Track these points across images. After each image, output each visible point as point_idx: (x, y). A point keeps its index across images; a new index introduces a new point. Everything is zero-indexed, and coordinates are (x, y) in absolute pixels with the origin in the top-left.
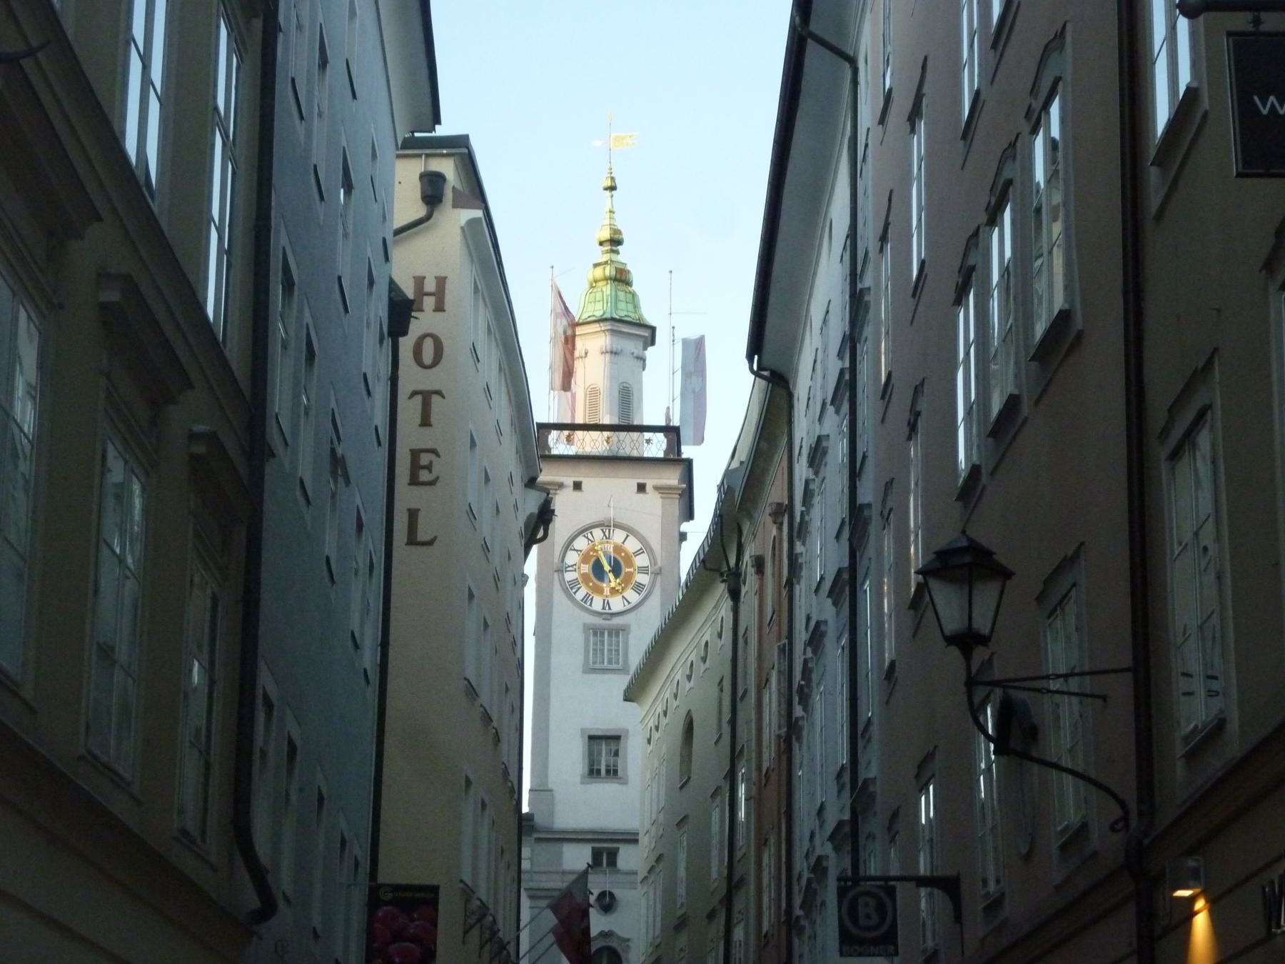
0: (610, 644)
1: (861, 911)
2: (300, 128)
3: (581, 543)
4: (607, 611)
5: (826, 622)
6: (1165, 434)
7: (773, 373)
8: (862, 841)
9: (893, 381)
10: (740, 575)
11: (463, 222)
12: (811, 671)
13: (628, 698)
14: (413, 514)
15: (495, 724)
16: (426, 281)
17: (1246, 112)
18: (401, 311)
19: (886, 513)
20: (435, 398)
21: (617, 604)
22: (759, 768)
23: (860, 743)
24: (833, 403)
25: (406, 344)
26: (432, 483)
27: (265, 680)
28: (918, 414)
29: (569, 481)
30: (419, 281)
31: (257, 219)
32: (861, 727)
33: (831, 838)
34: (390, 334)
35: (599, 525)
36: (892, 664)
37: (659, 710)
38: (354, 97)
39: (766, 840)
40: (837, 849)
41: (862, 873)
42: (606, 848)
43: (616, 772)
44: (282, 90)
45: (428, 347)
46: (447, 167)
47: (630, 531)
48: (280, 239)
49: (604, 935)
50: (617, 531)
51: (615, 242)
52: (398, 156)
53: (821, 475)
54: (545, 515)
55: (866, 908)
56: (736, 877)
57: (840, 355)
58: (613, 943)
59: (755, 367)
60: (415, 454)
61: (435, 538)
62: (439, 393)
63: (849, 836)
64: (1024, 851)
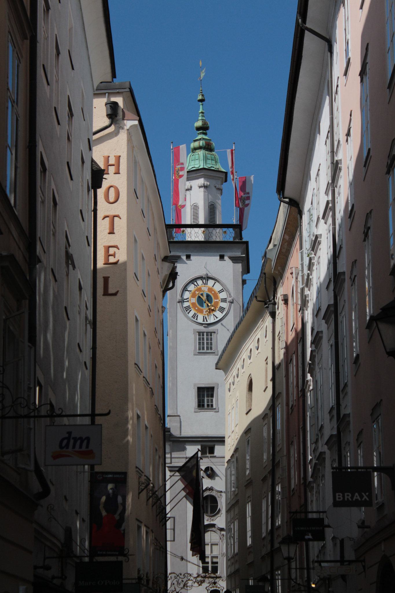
2: (47, 88)
3: (192, 287)
5: (322, 332)
7: (290, 199)
8: (343, 445)
9: (355, 209)
12: (315, 356)
13: (120, 156)
18: (97, 176)
19: (353, 277)
20: (116, 219)
21: (212, 320)
22: (288, 404)
23: (341, 396)
24: (323, 218)
25: (100, 192)
28: (369, 228)
32: (342, 386)
33: (327, 444)
35: (201, 278)
36: (358, 356)
38: (73, 69)
39: (292, 442)
41: (343, 465)
42: (209, 444)
44: (40, 72)
45: (112, 191)
52: (95, 94)
53: (318, 255)
54: (173, 276)
56: (277, 461)
57: (326, 193)
58: (214, 493)
61: (118, 291)
62: (118, 216)
63: (336, 442)
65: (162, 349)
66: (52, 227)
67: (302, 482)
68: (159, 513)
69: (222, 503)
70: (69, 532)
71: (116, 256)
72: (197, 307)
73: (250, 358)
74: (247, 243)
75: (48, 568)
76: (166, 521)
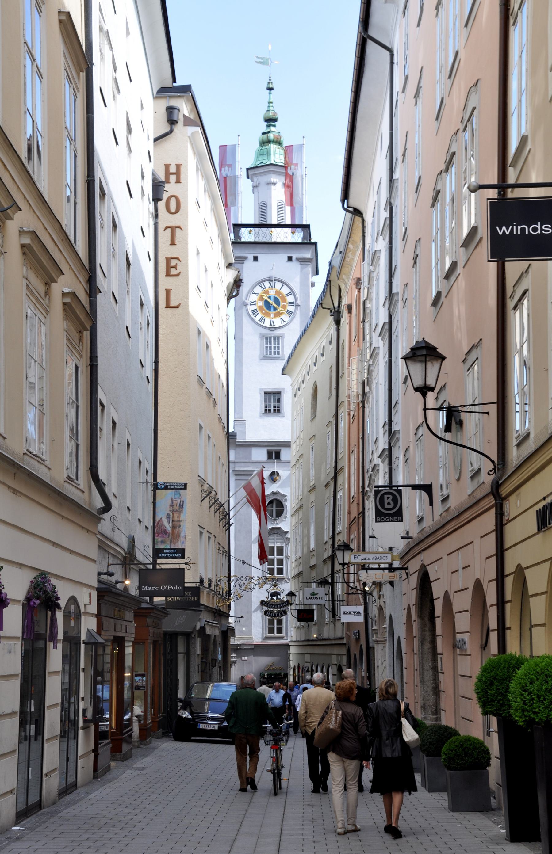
0: (275, 344)
1: (386, 501)
4: (272, 326)
6: (512, 296)
10: (340, 312)
11: (189, 134)
14: (168, 292)
15: (213, 396)
16: (171, 167)
17: (493, 232)
19: (404, 300)
20: (178, 230)
21: (278, 322)
25: (161, 205)
26: (177, 275)
27: (101, 395)
29: (251, 257)
30: (167, 166)
31: (88, 176)
33: (380, 456)
34: (153, 200)
35: (270, 280)
37: (300, 380)
40: (383, 462)
42: (274, 452)
43: (279, 410)
45: (173, 202)
46: (184, 108)
47: (284, 283)
48: (98, 174)
49: (274, 493)
50: (277, 283)
51: (271, 121)
55: (388, 500)
59: (346, 206)
60: (168, 260)
61: (180, 304)
64: (457, 478)
65: (226, 358)
66: (112, 250)
67: (361, 490)
68: (222, 519)
69: (290, 506)
70: (132, 541)
71: (178, 267)
72: (264, 310)
73: (315, 364)
74: (315, 244)
75: (111, 574)
76: (230, 526)
